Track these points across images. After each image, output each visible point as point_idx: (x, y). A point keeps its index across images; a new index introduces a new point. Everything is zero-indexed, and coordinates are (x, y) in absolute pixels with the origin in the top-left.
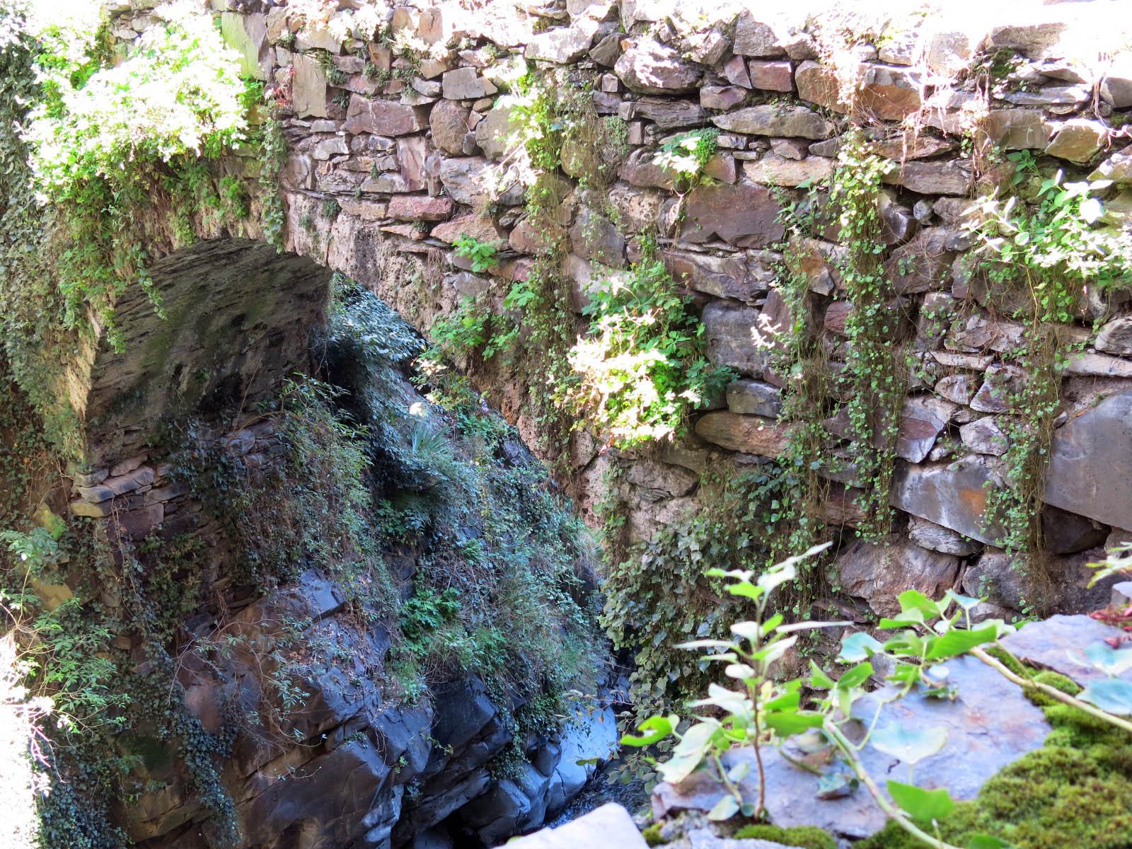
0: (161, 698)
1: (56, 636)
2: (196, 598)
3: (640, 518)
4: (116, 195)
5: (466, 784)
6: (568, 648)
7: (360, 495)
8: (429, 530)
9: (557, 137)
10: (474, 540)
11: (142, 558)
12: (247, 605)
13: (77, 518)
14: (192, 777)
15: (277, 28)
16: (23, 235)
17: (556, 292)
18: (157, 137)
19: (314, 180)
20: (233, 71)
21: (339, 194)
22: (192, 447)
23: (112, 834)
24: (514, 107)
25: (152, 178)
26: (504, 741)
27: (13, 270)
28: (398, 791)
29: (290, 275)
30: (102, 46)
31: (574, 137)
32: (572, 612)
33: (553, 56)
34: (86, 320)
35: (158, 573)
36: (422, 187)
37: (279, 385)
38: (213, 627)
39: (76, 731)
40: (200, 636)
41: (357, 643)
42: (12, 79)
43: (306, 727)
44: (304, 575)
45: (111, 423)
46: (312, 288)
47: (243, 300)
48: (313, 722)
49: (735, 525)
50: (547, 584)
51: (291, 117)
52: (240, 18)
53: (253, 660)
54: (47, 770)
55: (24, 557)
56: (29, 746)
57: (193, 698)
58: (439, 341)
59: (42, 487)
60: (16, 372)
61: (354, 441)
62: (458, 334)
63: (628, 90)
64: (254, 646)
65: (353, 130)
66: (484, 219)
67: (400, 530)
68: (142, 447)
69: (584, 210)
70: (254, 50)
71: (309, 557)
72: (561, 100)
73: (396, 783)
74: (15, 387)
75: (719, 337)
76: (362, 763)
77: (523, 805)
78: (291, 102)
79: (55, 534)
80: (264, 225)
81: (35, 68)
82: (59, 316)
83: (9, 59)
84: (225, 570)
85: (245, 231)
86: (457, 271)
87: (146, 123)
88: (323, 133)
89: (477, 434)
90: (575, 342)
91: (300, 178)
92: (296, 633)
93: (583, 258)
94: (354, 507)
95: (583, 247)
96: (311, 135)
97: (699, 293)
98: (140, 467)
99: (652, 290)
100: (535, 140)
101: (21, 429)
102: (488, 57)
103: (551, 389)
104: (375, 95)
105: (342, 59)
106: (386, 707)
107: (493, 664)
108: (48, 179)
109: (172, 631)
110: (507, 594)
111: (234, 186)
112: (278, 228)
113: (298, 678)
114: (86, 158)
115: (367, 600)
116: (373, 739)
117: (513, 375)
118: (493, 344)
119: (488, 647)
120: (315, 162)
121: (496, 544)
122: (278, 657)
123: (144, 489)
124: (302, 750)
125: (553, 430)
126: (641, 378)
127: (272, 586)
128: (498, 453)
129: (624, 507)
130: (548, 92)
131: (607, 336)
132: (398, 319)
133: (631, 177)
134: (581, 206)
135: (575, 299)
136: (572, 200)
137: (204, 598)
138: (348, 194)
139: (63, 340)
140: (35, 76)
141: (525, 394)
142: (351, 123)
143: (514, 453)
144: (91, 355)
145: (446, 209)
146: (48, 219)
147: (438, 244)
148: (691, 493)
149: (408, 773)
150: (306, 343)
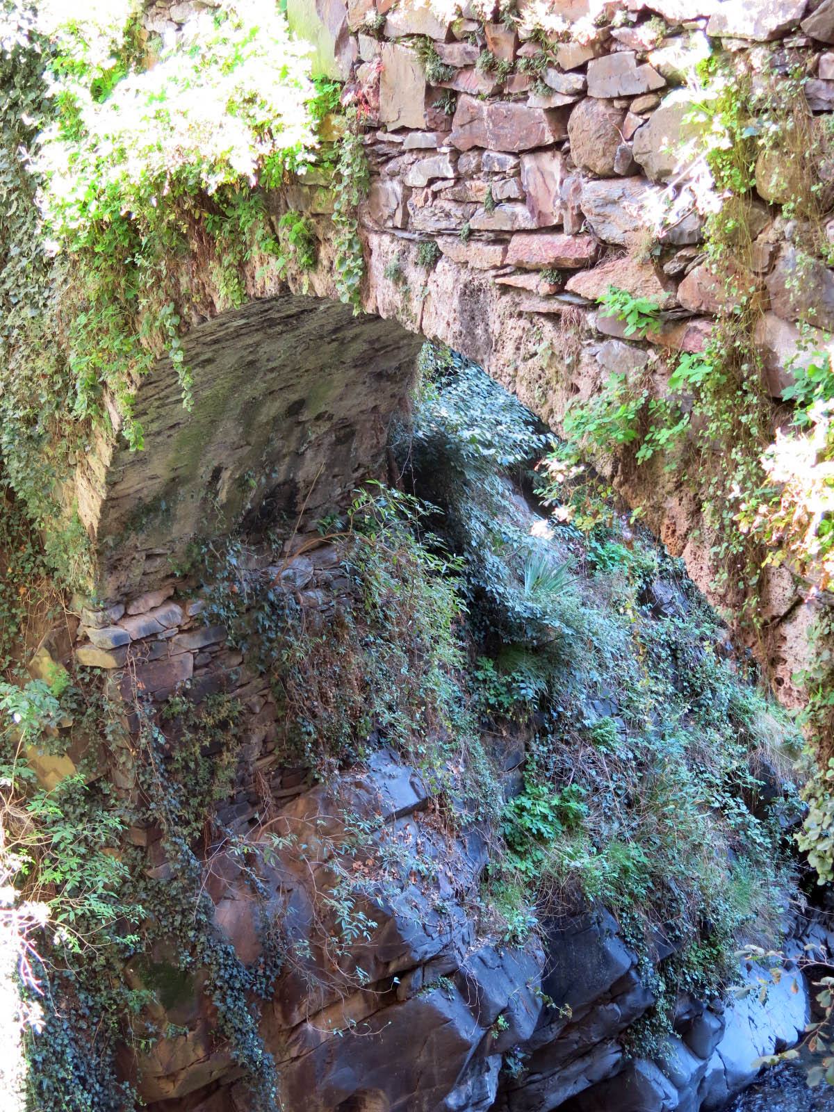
0: (183, 913)
1: (54, 823)
2: (232, 781)
4: (144, 240)
5: (588, 1061)
6: (737, 878)
7: (448, 652)
8: (545, 702)
9: (750, 147)
10: (607, 718)
11: (164, 725)
12: (298, 794)
13: (83, 669)
14: (221, 1022)
15: (361, 9)
16: (26, 295)
17: (745, 367)
18: (201, 162)
19: (406, 215)
20: (301, 69)
21: (440, 233)
22: (232, 579)
23: (118, 1090)
24: (690, 105)
25: (192, 216)
26: (643, 1005)
27: (12, 341)
28: (494, 1063)
29: (366, 346)
30: (131, 44)
31: (776, 146)
32: (745, 827)
33: (748, 31)
34: (102, 406)
35: (184, 745)
36: (555, 221)
37: (347, 497)
38: (253, 821)
39: (77, 950)
40: (237, 833)
41: (444, 854)
42: (18, 92)
43: (372, 966)
44: (374, 758)
45: (128, 543)
46: (395, 364)
47: (303, 380)
48: (382, 959)
50: (710, 785)
53: (303, 870)
54: (39, 999)
55: (17, 718)
56: (18, 966)
57: (225, 915)
58: (576, 437)
59: (41, 626)
60: (13, 475)
62: (600, 426)
64: (306, 851)
65: (462, 144)
66: (643, 264)
67: (505, 699)
68: (168, 577)
69: (788, 250)
70: (330, 40)
71: (381, 733)
72: (759, 93)
73: (493, 1052)
74: (11, 494)
76: (447, 1021)
77: (667, 1097)
78: (378, 109)
79: (56, 690)
80: (337, 277)
81: (47, 77)
82: (68, 401)
83: (15, 67)
84: (270, 746)
85: (311, 286)
86: (602, 338)
87: (187, 143)
88: (419, 150)
89: (615, 570)
90: (771, 439)
91: (387, 212)
92: (362, 837)
94: (442, 666)
95: (786, 303)
96: (402, 153)
100: (719, 152)
101: (17, 549)
102: (653, 36)
103: (737, 503)
104: (492, 95)
106: (481, 946)
107: (631, 894)
108: (60, 221)
109: (200, 825)
110: (653, 796)
111: (298, 226)
112: (356, 281)
113: (364, 898)
114: (108, 192)
115: (459, 795)
116: (462, 989)
117: (679, 485)
118: (651, 441)
119: (625, 870)
120: (408, 190)
121: (638, 726)
122: (337, 868)
123: (168, 633)
124: (366, 998)
125: (736, 563)
127: (332, 771)
130: (739, 83)
131: (820, 430)
132: (510, 407)
134: (784, 244)
135: (772, 377)
136: (771, 235)
137: (242, 782)
138: (452, 233)
139: (73, 434)
140: (47, 87)
141: (696, 512)
142: (458, 135)
143: (667, 598)
144: (106, 452)
145: (588, 251)
146: (57, 273)
147: (576, 301)
149: (509, 1038)
150: (383, 439)
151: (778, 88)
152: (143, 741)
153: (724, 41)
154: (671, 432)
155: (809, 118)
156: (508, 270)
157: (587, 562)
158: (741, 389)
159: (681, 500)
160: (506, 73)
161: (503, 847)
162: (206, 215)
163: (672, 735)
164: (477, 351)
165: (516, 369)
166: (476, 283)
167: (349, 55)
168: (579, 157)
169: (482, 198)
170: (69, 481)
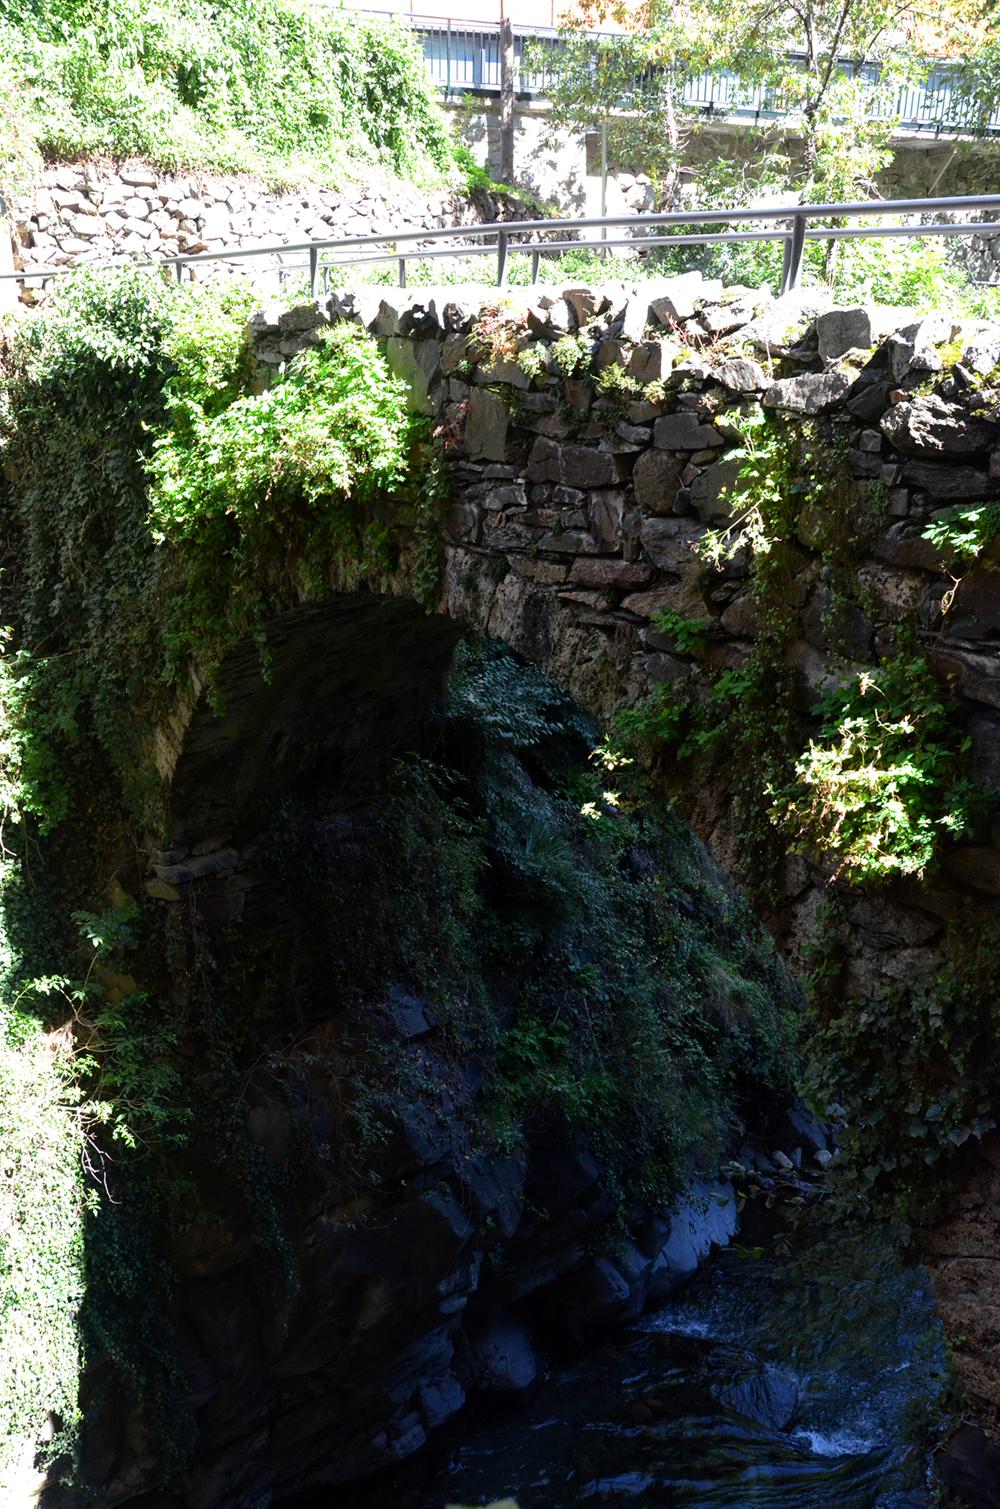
3: (861, 967)
6: (688, 1106)
7: (470, 900)
13: (150, 900)
19: (481, 533)
21: (510, 551)
24: (744, 462)
28: (478, 1256)
31: (818, 503)
32: (699, 1064)
34: (187, 676)
38: (286, 1040)
44: (392, 989)
49: (989, 988)
51: (459, 459)
52: (410, 345)
61: (469, 836)
63: (894, 450)
64: (331, 1067)
65: (535, 477)
66: (695, 590)
69: (823, 590)
75: (988, 755)
77: (620, 1290)
85: (389, 586)
88: (497, 479)
93: (817, 648)
97: (967, 700)
98: (223, 846)
99: (906, 692)
105: (530, 397)
107: (602, 1116)
108: (168, 516)
111: (383, 535)
112: (431, 586)
117: (710, 780)
119: (597, 1097)
120: (484, 513)
125: (757, 849)
126: (889, 797)
128: (625, 862)
129: (840, 953)
133: (889, 553)
134: (819, 585)
138: (521, 551)
141: (725, 804)
143: (643, 864)
144: (186, 714)
145: (643, 576)
147: (630, 617)
148: (931, 943)
151: (825, 455)
152: (198, 965)
153: (778, 412)
154: (709, 735)
155: (850, 481)
156: (570, 587)
157: (578, 831)
158: (774, 703)
159: (712, 792)
160: (581, 422)
161: (496, 1071)
162: (299, 519)
163: (643, 982)
164: (537, 653)
165: (571, 671)
166: (540, 595)
167: (440, 394)
168: (642, 496)
169: (552, 524)
170: (149, 737)
